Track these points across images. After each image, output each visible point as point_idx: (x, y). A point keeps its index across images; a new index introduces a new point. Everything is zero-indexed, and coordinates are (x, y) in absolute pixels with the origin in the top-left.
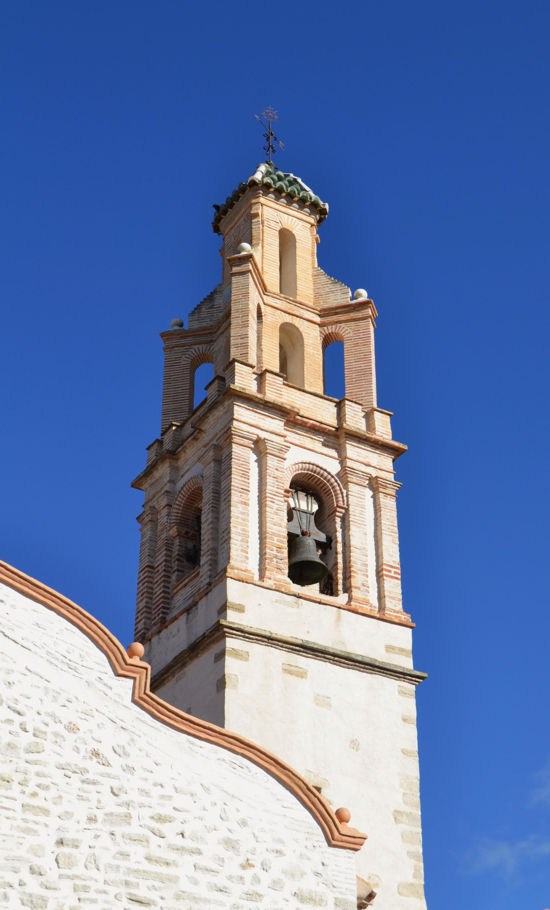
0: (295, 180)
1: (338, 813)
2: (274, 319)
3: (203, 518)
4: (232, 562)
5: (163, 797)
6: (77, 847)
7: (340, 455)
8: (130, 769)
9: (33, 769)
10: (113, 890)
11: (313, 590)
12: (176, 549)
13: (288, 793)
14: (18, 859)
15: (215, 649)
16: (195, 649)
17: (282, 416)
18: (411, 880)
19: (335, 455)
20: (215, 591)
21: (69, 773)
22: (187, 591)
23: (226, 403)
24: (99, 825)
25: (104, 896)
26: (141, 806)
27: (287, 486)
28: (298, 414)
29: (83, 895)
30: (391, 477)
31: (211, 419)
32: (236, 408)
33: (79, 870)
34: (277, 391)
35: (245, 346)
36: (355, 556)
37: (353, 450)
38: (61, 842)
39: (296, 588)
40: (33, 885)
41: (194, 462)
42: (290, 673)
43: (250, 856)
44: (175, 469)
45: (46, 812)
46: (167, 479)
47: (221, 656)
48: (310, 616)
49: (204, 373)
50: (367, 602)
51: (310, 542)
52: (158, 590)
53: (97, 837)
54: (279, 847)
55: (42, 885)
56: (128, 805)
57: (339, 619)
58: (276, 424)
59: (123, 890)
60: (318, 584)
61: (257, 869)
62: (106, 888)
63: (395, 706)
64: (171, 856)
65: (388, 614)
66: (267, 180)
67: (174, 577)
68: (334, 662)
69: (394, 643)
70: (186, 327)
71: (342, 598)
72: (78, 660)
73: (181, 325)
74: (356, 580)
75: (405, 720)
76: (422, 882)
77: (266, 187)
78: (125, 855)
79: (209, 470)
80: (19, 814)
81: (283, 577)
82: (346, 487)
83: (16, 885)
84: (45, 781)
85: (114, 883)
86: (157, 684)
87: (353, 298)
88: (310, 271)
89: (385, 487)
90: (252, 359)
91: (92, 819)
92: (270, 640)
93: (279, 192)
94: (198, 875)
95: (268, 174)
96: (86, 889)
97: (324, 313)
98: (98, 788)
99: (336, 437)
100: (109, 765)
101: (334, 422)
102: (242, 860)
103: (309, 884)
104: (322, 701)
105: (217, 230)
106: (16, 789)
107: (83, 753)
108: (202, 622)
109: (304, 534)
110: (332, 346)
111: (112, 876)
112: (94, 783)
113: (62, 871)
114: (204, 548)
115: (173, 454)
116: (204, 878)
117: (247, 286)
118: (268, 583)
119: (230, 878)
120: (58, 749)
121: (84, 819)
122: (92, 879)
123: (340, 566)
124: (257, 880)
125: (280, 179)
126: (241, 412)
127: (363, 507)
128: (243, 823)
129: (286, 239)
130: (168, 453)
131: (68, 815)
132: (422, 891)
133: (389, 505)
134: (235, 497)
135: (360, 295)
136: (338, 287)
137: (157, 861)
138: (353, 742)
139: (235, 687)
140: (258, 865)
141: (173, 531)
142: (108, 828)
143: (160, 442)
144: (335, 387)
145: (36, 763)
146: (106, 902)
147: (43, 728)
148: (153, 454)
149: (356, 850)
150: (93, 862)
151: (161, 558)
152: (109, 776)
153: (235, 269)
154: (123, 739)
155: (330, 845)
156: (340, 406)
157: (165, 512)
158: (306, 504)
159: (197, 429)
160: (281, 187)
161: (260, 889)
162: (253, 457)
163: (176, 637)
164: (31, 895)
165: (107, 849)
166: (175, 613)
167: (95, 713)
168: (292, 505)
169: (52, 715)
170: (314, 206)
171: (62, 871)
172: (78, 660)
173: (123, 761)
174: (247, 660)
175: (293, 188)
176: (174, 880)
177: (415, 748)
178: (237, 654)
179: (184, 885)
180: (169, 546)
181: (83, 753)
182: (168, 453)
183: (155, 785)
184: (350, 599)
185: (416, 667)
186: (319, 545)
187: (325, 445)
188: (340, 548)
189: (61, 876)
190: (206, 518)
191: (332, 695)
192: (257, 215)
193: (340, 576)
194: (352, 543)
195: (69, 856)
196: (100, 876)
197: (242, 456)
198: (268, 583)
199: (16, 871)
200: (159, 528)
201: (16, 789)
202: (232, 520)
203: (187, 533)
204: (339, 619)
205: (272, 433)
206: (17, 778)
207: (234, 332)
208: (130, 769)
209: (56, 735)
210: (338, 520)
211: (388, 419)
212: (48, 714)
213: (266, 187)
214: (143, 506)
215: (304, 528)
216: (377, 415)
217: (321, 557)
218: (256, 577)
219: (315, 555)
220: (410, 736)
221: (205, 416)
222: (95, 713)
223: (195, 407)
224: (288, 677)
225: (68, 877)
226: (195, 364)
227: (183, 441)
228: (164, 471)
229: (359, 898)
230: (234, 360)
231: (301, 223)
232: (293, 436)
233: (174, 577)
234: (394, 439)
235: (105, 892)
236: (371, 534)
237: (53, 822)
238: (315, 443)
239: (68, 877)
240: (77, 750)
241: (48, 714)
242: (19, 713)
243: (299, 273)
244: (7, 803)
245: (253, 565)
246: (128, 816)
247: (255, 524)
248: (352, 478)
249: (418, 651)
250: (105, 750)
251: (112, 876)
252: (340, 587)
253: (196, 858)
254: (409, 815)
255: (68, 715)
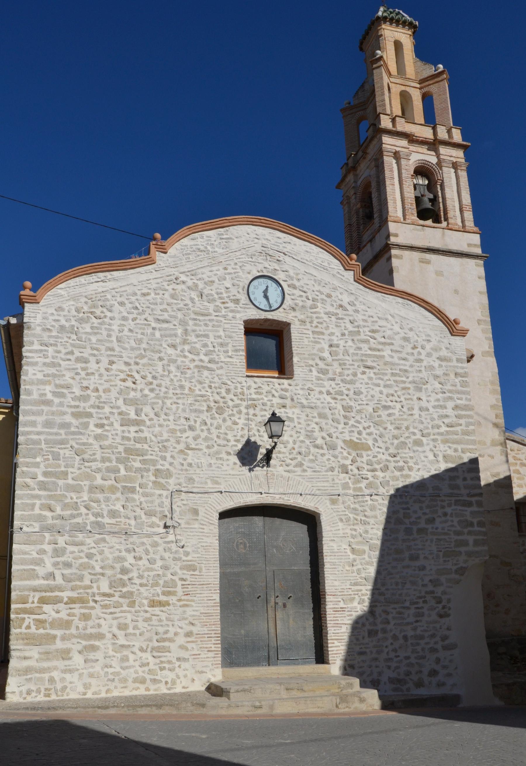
0: (399, 12)
1: (454, 320)
2: (396, 89)
3: (373, 196)
4: (390, 214)
5: (373, 322)
6: (338, 347)
7: (436, 154)
8: (357, 311)
9: (314, 316)
10: (356, 364)
11: (429, 222)
13: (430, 314)
14: (314, 354)
15: (386, 256)
16: (377, 258)
17: (406, 138)
18: (487, 349)
19: (434, 154)
20: (383, 229)
22: (369, 232)
23: (378, 136)
24: (347, 337)
25: (353, 367)
26: (364, 326)
27: (412, 173)
28: (414, 136)
29: (343, 367)
30: (463, 161)
31: (371, 146)
32: (383, 138)
33: (341, 356)
34: (402, 126)
35: (384, 105)
36: (449, 203)
37: (443, 150)
38: (331, 346)
39: (422, 222)
40: (322, 365)
41: (365, 170)
44: (356, 176)
45: (323, 334)
46: (352, 181)
47: (389, 259)
48: (431, 235)
49: (364, 125)
50: (457, 224)
51: (426, 199)
52: (355, 234)
53: (346, 342)
54: (428, 338)
55: (326, 364)
57: (443, 234)
58: (404, 143)
59: (360, 363)
61: (420, 349)
62: (353, 363)
63: (474, 273)
64: (380, 347)
65: (467, 228)
66: (385, 14)
67: (362, 227)
68: (443, 255)
69: (472, 241)
70: (352, 104)
71: (444, 224)
73: (349, 103)
74: (450, 214)
75: (479, 278)
76: (493, 350)
77: (385, 19)
79: (373, 172)
81: (415, 218)
82: (441, 169)
84: (321, 320)
85: (356, 361)
86: (365, 271)
87: (435, 71)
88: (412, 61)
89: (461, 166)
90: (388, 112)
92: (412, 248)
93: (391, 21)
94: (393, 354)
95: (385, 11)
96: (345, 364)
97: (421, 82)
98: (345, 321)
99: (433, 145)
100: (348, 310)
101: (432, 137)
103: (444, 353)
104: (439, 273)
105: (361, 49)
107: (335, 306)
108: (378, 244)
109: (422, 196)
110: (427, 99)
111: (355, 358)
112: (342, 319)
115: (354, 168)
117: (381, 74)
118: (408, 221)
119: (408, 354)
121: (339, 335)
123: (442, 208)
124: (419, 353)
125: (391, 13)
126: (386, 139)
127: (450, 178)
129: (398, 45)
130: (351, 168)
131: (332, 334)
132: (493, 354)
133: (463, 175)
134: (388, 182)
135: (439, 68)
136: (427, 66)
139: (398, 272)
140: (419, 347)
141: (359, 206)
142: (351, 338)
143: (347, 164)
144: (430, 119)
146: (354, 369)
147: (316, 297)
148: (344, 171)
151: (354, 219)
152: (348, 315)
153: (374, 66)
154: (352, 298)
155: (452, 335)
156: (434, 129)
157: (353, 197)
158: (422, 181)
159: (365, 153)
160: (392, 17)
161: (422, 357)
162: (394, 161)
163: (368, 253)
164: (321, 369)
165: (351, 347)
166: (364, 243)
168: (415, 183)
170: (411, 25)
171: (334, 358)
173: (354, 308)
174: (402, 259)
175: (400, 16)
176: (383, 357)
177: (485, 290)
178: (397, 257)
179: (388, 359)
180: (357, 213)
181: (335, 306)
182: (351, 168)
183: (369, 317)
184: (448, 224)
185: (483, 252)
186: (430, 200)
187: (428, 150)
189: (333, 360)
190: (374, 195)
191: (446, 269)
192: (381, 35)
193: (442, 214)
195: (336, 351)
197: (389, 161)
198: (408, 221)
199: (313, 359)
200: (352, 205)
201: (308, 325)
202: (388, 193)
204: (443, 234)
205: (402, 147)
206: (308, 320)
207: (377, 99)
208: (357, 311)
209: (322, 300)
210: (439, 187)
211: (459, 131)
212: (317, 291)
213: (385, 19)
215: (422, 193)
216: (454, 130)
217: (432, 206)
218: (402, 220)
219: (429, 205)
220: (482, 285)
221: (367, 147)
223: (361, 142)
225: (336, 360)
226: (359, 122)
227: (358, 162)
228: (350, 177)
230: (380, 113)
231: (404, 35)
232: (412, 148)
233: (362, 227)
234: (463, 140)
235: (353, 365)
236: (456, 192)
237: (326, 337)
238: (424, 149)
239: (336, 360)
240: (333, 305)
241: (317, 291)
243: (406, 63)
244: (305, 331)
245: (400, 214)
247: (399, 194)
248: (444, 164)
249: (484, 245)
251: (355, 358)
252: (443, 219)
254: (485, 321)
255: (326, 291)
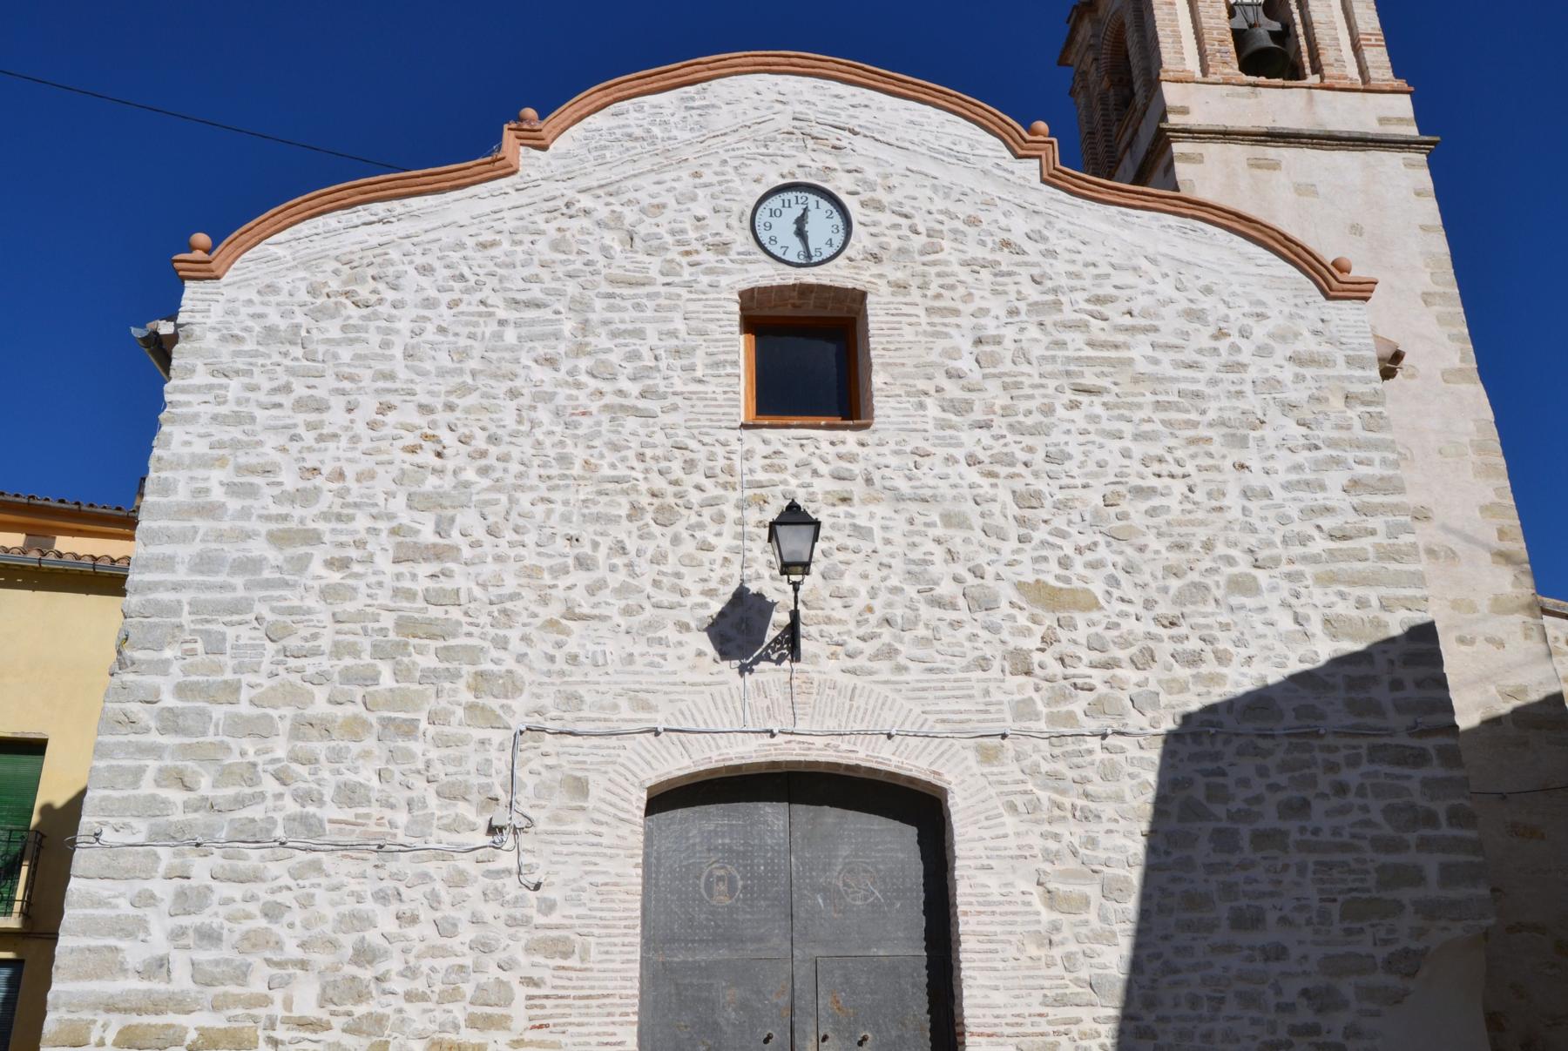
5: (1098, 276)
8: (1052, 254)
9: (933, 270)
10: (1052, 384)
12: (1112, 101)
13: (1260, 250)
14: (931, 365)
15: (1163, 162)
20: (1154, 100)
21: (976, 268)
25: (1042, 391)
29: (1015, 392)
33: (1007, 366)
36: (1320, 32)
38: (979, 341)
42: (1259, 167)
43: (1222, 325)
45: (956, 312)
53: (1022, 330)
54: (1259, 310)
55: (963, 388)
56: (1055, 291)
57: (1311, 100)
60: (1467, 717)
61: (1235, 338)
62: (1043, 381)
64: (1120, 338)
68: (1314, 146)
72: (967, 150)
74: (1327, 57)
75: (1418, 194)
78: (1061, 344)
80: (924, 319)
81: (1233, 69)
83: (932, 392)
85: (1052, 375)
91: (1013, 312)
94: (1159, 354)
96: (1018, 386)
98: (1017, 278)
100: (1024, 253)
102: (1212, 330)
106: (915, 294)
107: (990, 245)
109: (1251, 26)
111: (1048, 368)
112: (1010, 274)
113: (987, 371)
114: (1135, 72)
116: (1165, 357)
119: (1200, 351)
120: (961, 247)
121: (1003, 314)
122: (1023, 374)
128: (1207, 290)
131: (984, 312)
132: (1476, 376)
137: (1103, 345)
138: (1353, 227)
141: (1105, 84)
145: (934, 263)
146: (1045, 396)
147: (938, 227)
149: (1366, 299)
150: (1022, 355)
152: (1026, 264)
154: (1037, 223)
155: (1328, 297)
157: (1093, 69)
161: (1244, 357)
164: (951, 400)
165: (1037, 340)
167: (998, 202)
169: (946, 212)
171: (987, 371)
172: (967, 150)
174: (1201, 162)
176: (1130, 361)
177: (1439, 221)
178: (1187, 158)
179: (1142, 366)
180: (1103, 100)
181: (990, 245)
183: (1086, 265)
184: (1322, 78)
185: (1421, 132)
188: (1300, 30)
189: (985, 377)
193: (1306, 59)
194: (1314, 18)
195: (992, 354)
196: (1033, 370)
201: (915, 294)
203: (1121, 80)
204: (1311, 100)
209: (955, 231)
212: (941, 212)
214: (1063, 61)
218: (1198, 75)
220: (1429, 210)
222: (998, 202)
224: (1258, 172)
225: (994, 376)
228: (1086, 29)
229: (1381, 360)
235: (1042, 386)
239: (994, 376)
240: (983, 243)
241: (941, 212)
242: (906, 216)
246: (1058, 303)
249: (1422, 117)
250: (1017, 237)
251: (1048, 368)
252: (1308, 71)
253: (1152, 337)
254: (1443, 295)
